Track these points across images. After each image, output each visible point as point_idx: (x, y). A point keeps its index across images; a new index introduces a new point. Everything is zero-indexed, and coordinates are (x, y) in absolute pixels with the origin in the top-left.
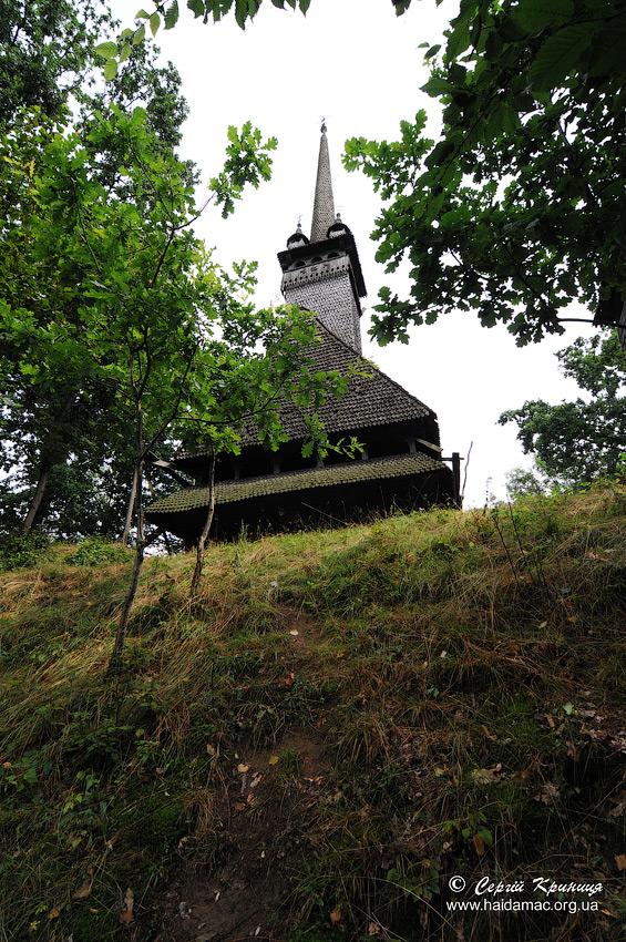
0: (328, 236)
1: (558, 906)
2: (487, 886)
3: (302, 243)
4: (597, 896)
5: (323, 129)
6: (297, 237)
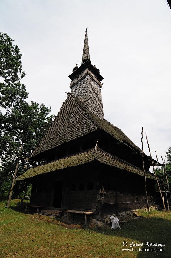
1: (153, 250)
2: (133, 244)
4: (163, 247)
5: (86, 32)
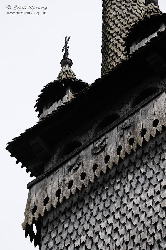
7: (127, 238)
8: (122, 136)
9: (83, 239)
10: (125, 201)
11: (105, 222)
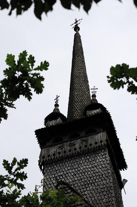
0: (85, 113)
3: (59, 120)
5: (77, 28)
6: (56, 115)
7: (79, 178)
8: (82, 143)
9: (62, 173)
10: (80, 166)
11: (71, 171)
